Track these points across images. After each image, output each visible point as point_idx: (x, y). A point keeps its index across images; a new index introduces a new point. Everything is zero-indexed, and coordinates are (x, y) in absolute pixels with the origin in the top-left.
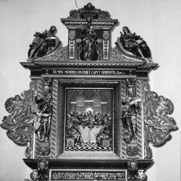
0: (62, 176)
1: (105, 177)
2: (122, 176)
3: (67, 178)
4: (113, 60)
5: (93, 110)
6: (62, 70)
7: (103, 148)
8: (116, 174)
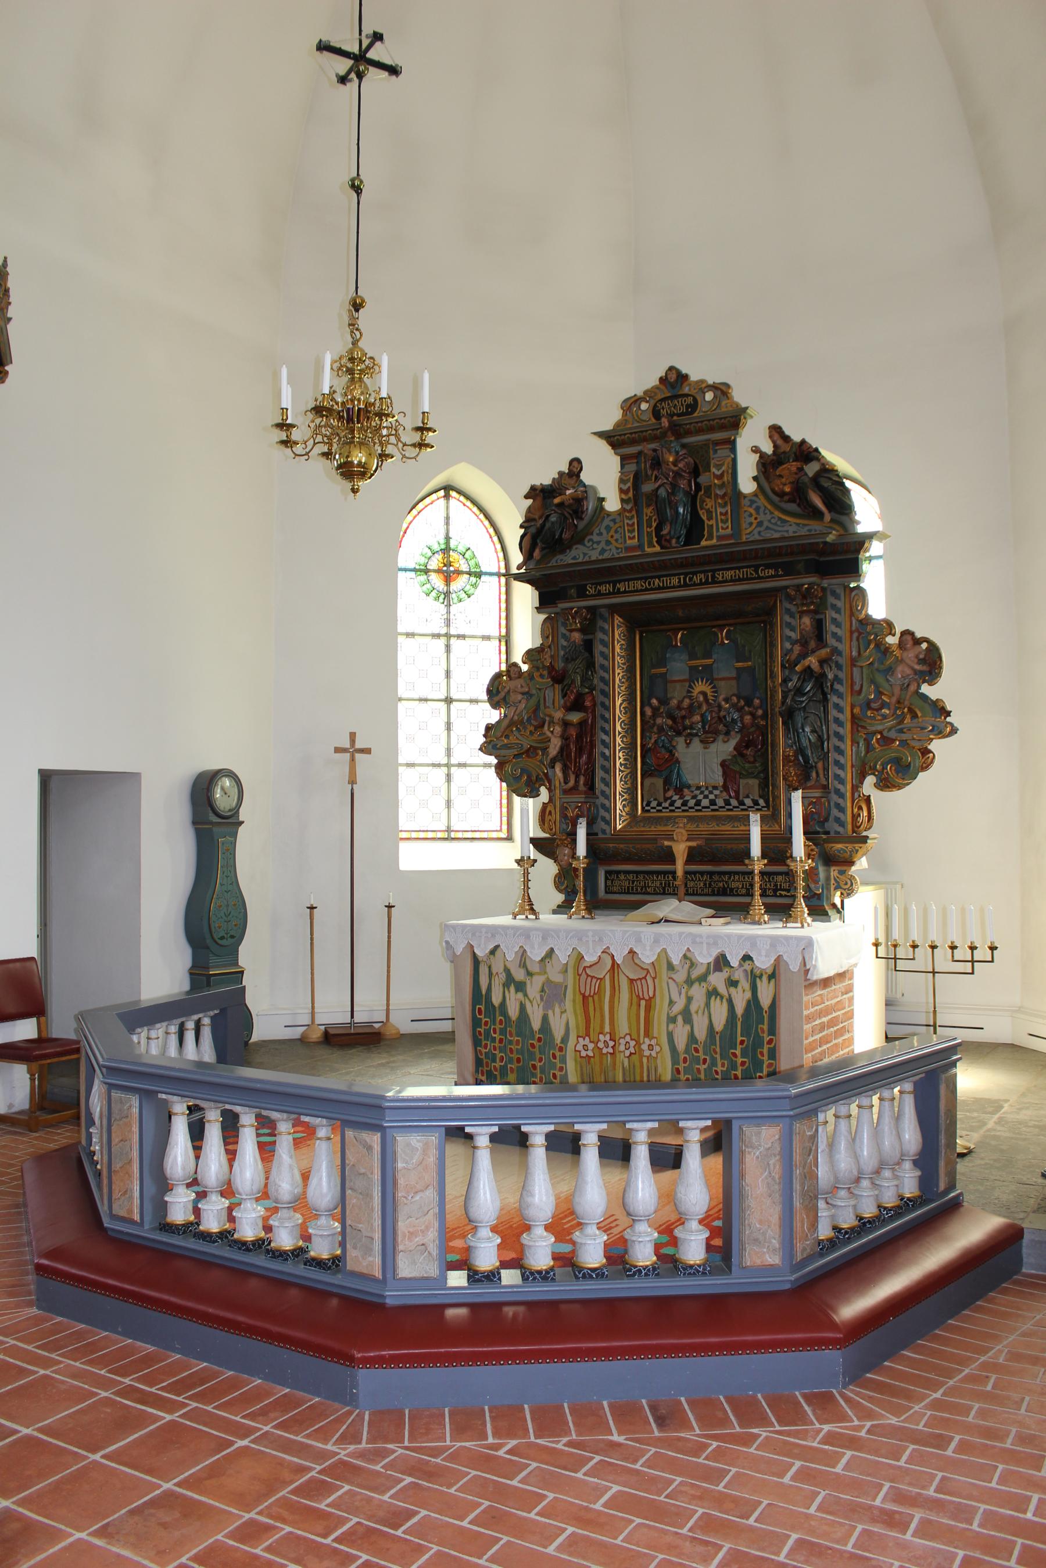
1: (743, 887)
6: (609, 583)
7: (742, 803)
8: (773, 878)
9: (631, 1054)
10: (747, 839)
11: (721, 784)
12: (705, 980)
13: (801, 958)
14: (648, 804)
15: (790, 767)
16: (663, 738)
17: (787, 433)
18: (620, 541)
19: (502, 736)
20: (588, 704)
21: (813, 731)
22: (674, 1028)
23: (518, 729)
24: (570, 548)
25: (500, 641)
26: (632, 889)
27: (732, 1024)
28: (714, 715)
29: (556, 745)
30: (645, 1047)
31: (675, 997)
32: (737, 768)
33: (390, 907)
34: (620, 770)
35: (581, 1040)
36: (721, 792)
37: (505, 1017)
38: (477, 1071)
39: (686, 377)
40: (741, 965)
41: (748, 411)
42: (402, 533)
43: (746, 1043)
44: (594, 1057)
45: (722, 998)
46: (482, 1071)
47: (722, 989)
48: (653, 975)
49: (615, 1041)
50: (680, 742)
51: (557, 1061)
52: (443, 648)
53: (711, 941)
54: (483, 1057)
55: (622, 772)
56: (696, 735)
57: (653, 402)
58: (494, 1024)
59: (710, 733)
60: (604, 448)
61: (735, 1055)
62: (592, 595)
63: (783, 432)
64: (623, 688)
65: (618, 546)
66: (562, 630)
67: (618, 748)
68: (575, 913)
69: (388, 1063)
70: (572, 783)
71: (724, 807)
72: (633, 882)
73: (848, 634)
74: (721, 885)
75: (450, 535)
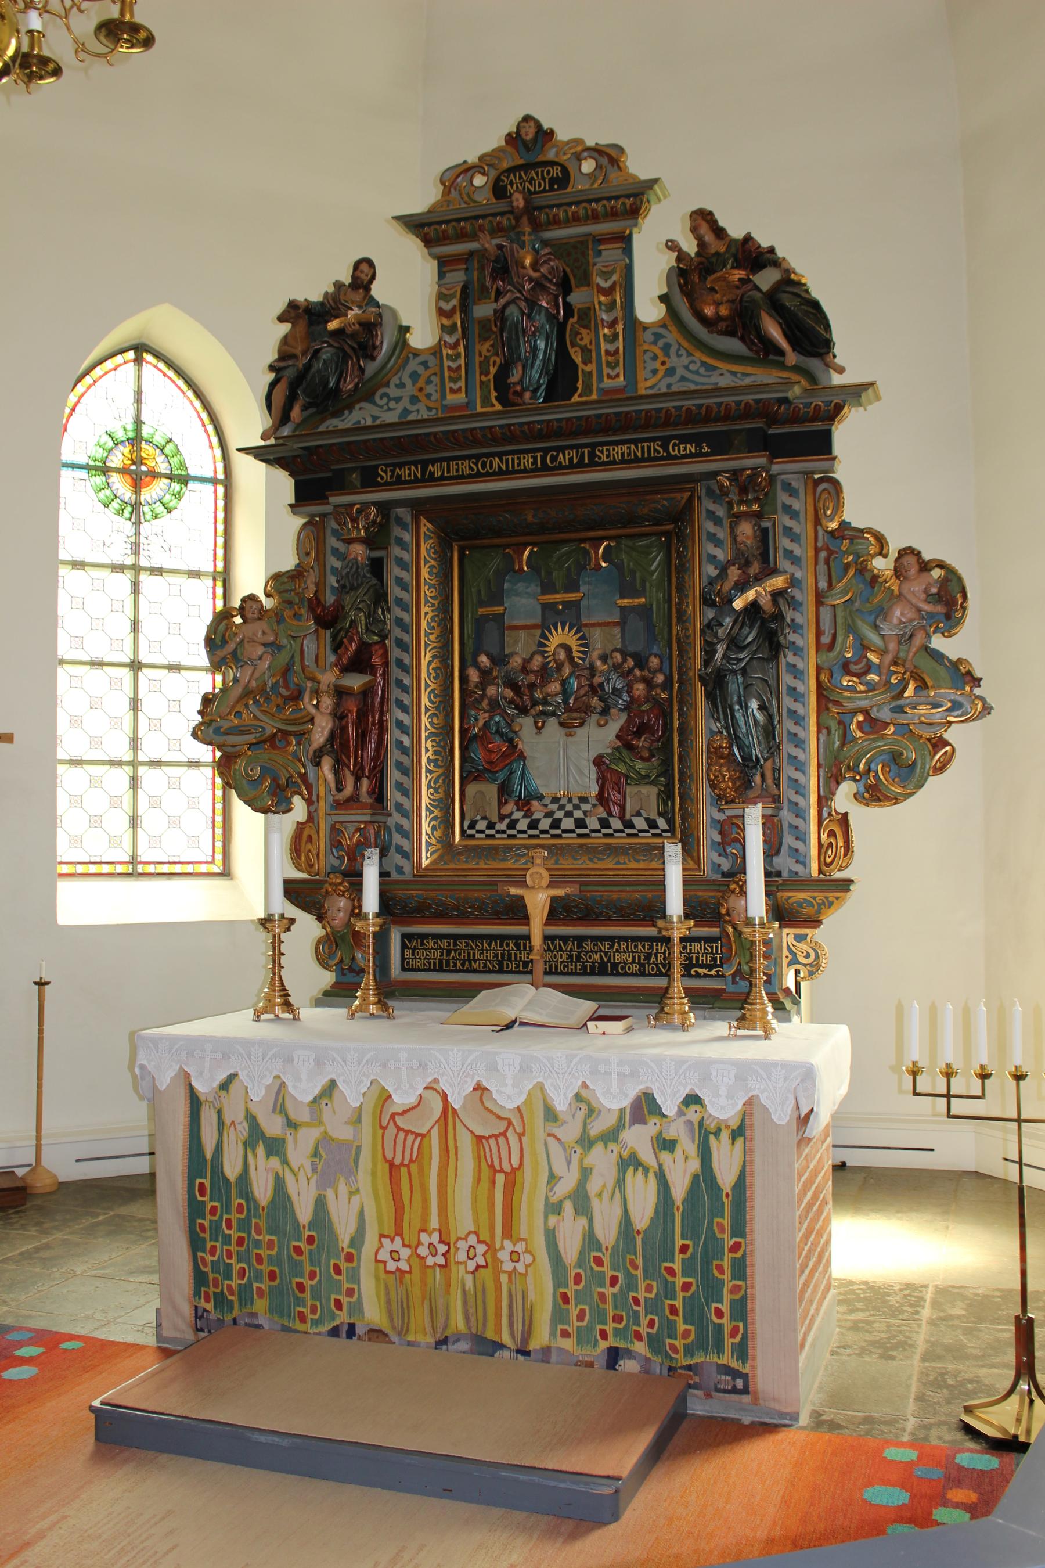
0: (442, 955)
1: (633, 961)
2: (714, 959)
3: (463, 965)
4: (651, 387)
5: (579, 639)
6: (415, 463)
7: (629, 825)
9: (478, 1267)
10: (660, 884)
11: (594, 794)
12: (615, 1140)
13: (794, 1101)
14: (472, 826)
15: (721, 766)
16: (497, 719)
17: (722, 223)
18: (433, 398)
19: (229, 713)
20: (376, 660)
21: (762, 708)
22: (558, 1222)
23: (256, 702)
24: (350, 407)
25: (215, 580)
26: (448, 965)
27: (665, 1214)
28: (584, 682)
29: (323, 728)
30: (504, 1255)
31: (559, 1168)
32: (622, 768)
33: (41, 984)
34: (427, 770)
35: (386, 1242)
36: (594, 806)
37: (248, 1201)
38: (197, 1293)
39: (548, 135)
40: (681, 1113)
41: (656, 187)
42: (67, 411)
43: (690, 1250)
44: (410, 1272)
45: (646, 1170)
46: (207, 1294)
47: (647, 1156)
48: (519, 1130)
49: (448, 1244)
50: (526, 725)
51: (343, 1278)
52: (128, 587)
53: (627, 1070)
54: (209, 1269)
55: (431, 772)
56: (553, 714)
57: (493, 174)
58: (228, 1211)
59: (576, 710)
60: (412, 247)
61: (671, 1272)
62: (386, 484)
63: (716, 222)
64: (432, 637)
65: (431, 405)
66: (333, 542)
67: (424, 734)
68: (360, 1009)
69: (37, 1250)
70: (349, 790)
71: (598, 831)
72: (449, 952)
73: (811, 553)
74: (597, 957)
75: (143, 418)
